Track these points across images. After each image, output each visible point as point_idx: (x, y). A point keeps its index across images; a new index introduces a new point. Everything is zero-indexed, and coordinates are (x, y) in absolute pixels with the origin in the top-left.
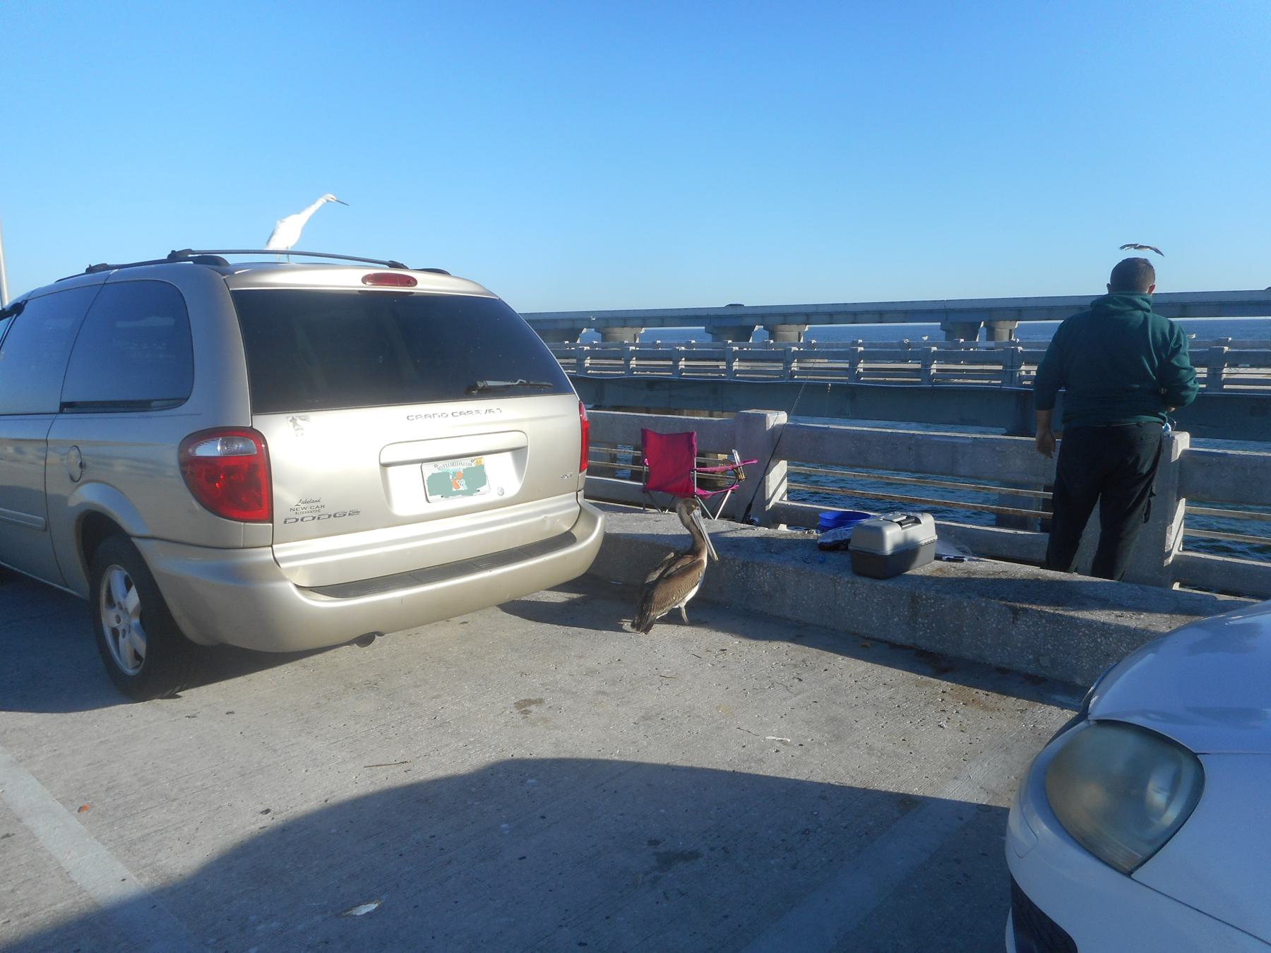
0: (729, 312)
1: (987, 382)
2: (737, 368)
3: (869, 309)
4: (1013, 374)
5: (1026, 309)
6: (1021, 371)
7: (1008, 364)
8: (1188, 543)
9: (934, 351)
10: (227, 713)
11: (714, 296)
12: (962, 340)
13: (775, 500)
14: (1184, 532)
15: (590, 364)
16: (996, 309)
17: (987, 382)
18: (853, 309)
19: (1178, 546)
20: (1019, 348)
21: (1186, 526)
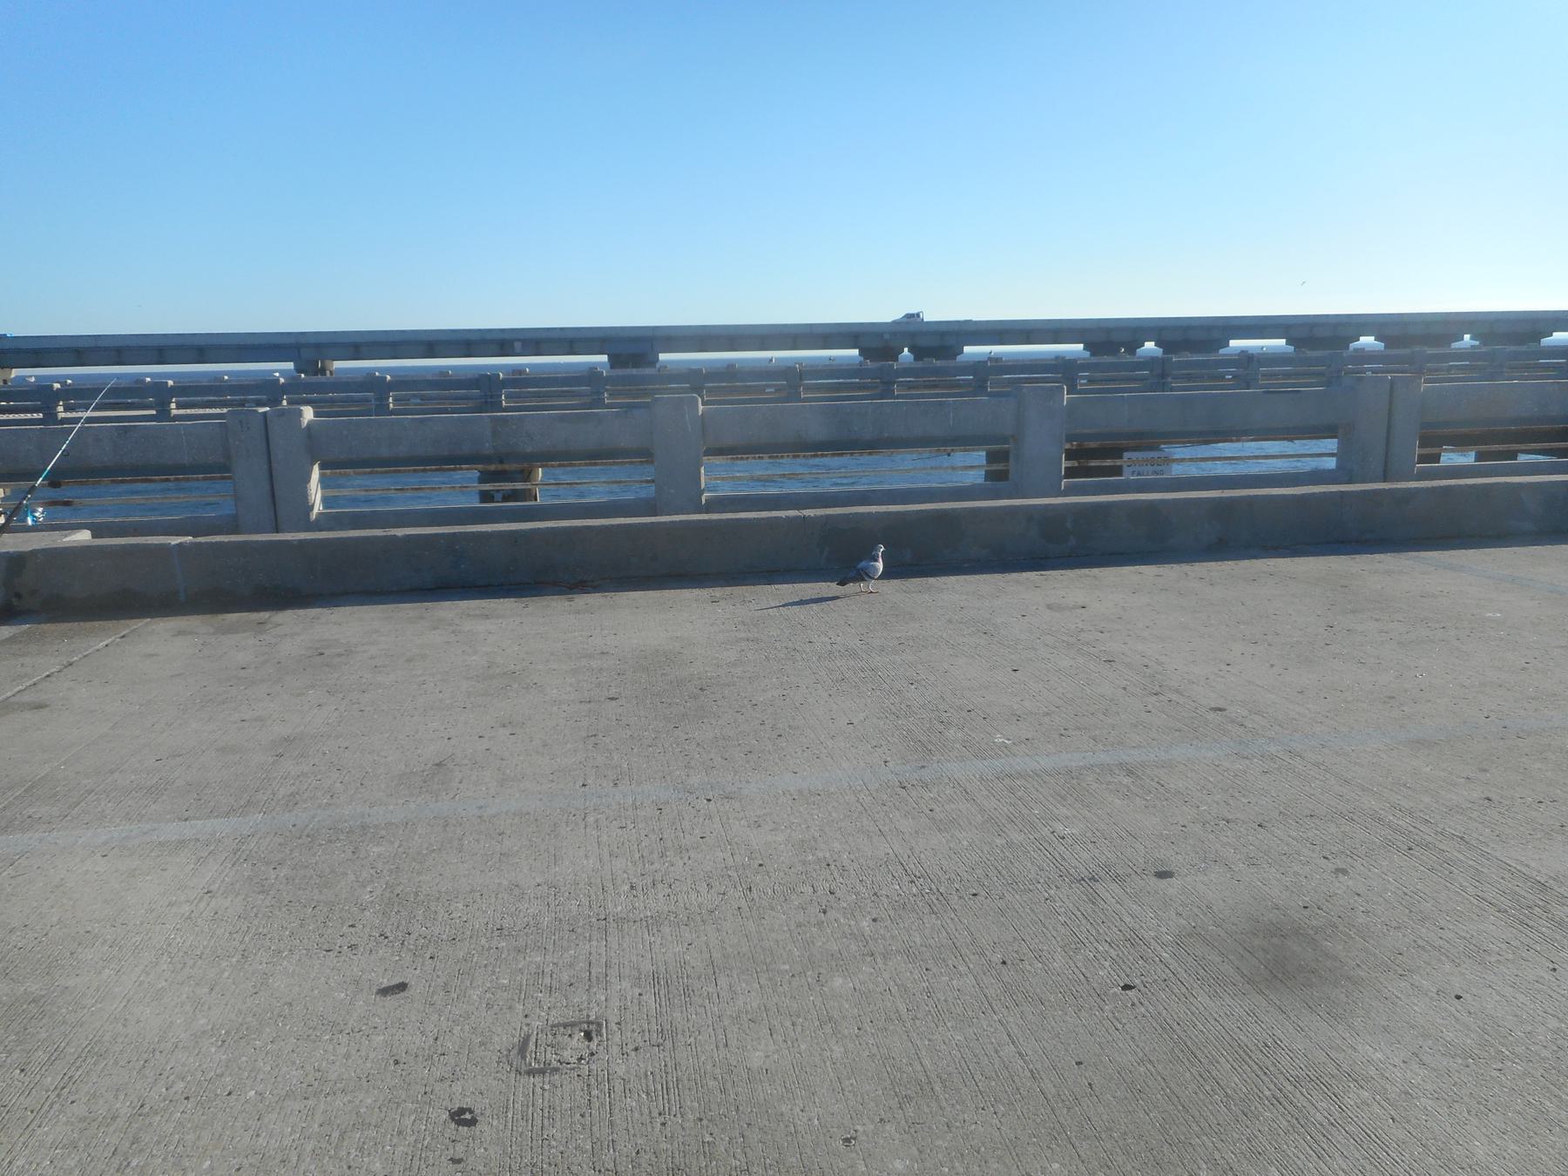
8: (325, 500)
21: (322, 488)
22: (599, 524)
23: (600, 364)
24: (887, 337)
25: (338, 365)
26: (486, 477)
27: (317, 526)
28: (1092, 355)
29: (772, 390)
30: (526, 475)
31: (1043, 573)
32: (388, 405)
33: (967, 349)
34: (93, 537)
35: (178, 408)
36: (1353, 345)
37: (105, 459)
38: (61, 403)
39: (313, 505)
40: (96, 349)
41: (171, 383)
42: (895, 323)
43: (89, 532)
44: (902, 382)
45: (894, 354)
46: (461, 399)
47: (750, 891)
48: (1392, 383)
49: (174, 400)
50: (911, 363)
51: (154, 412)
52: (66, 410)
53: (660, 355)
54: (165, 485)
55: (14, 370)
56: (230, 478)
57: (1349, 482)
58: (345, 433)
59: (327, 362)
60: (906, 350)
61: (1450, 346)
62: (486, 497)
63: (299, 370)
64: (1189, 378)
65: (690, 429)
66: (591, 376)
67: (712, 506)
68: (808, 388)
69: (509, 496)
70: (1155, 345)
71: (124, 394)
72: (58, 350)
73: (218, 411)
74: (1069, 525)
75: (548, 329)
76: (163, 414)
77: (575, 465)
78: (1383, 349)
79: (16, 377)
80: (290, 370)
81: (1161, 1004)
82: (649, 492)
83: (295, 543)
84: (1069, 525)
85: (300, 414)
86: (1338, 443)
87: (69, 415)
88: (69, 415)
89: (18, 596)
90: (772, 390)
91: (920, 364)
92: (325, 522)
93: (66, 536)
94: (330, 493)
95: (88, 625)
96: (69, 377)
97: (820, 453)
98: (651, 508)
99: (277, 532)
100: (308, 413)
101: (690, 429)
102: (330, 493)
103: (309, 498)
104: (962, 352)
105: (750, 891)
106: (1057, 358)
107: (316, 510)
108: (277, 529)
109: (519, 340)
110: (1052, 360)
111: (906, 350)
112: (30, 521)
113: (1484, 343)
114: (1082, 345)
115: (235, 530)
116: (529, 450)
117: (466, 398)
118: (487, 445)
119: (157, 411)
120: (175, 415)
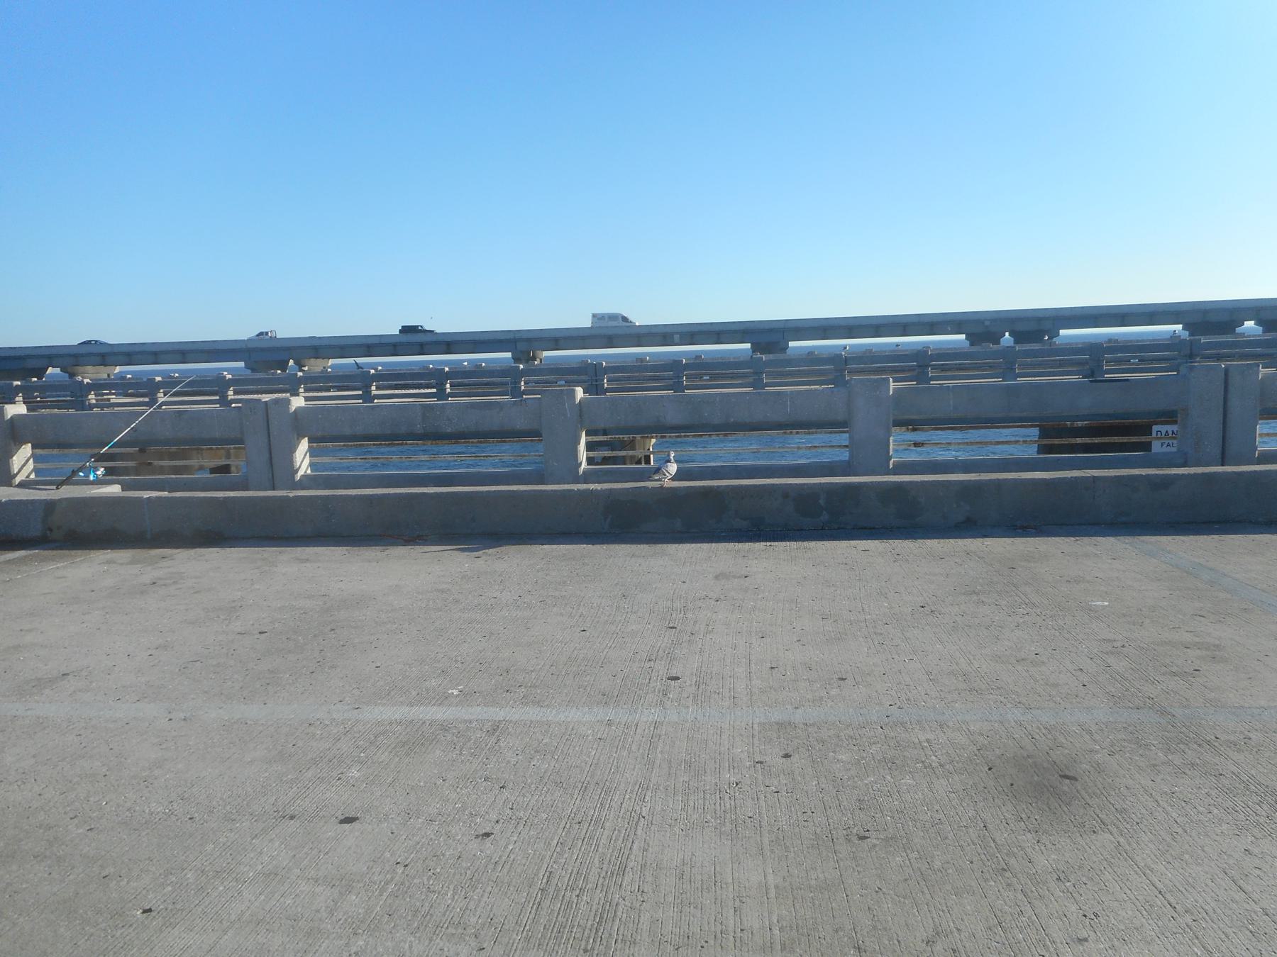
0: (85, 350)
1: (1077, 377)
2: (233, 397)
3: (170, 349)
4: (83, 402)
5: (457, 342)
6: (89, 400)
7: (78, 395)
8: (590, 461)
9: (373, 374)
10: (260, 633)
11: (240, 329)
12: (279, 372)
13: (301, 473)
14: (587, 455)
15: (97, 400)
16: (536, 340)
17: (1077, 377)
18: (154, 349)
19: (305, 469)
20: (156, 378)
21: (587, 451)
22: (737, 484)
23: (746, 350)
24: (987, 323)
25: (546, 354)
26: (1044, 433)
27: (302, 485)
28: (972, 344)
29: (705, 378)
30: (1146, 429)
31: (772, 543)
32: (603, 384)
33: (1063, 332)
34: (122, 491)
35: (234, 394)
36: (1238, 330)
37: (167, 433)
38: (302, 386)
39: (581, 463)
40: (860, 327)
41: (447, 369)
42: (250, 340)
43: (120, 486)
44: (935, 365)
45: (996, 338)
46: (1163, 360)
47: (338, 780)
48: (1226, 371)
49: (374, 384)
50: (1259, 336)
51: (361, 393)
52: (234, 394)
53: (1061, 331)
54: (400, 448)
55: (118, 367)
56: (244, 448)
57: (1185, 465)
58: (320, 416)
59: (539, 352)
60: (1007, 334)
61: (1235, 330)
62: (1044, 449)
63: (516, 359)
64: (943, 368)
65: (569, 415)
66: (1173, 344)
67: (902, 468)
68: (934, 367)
69: (177, 470)
70: (61, 371)
71: (199, 386)
72: (462, 342)
73: (141, 399)
74: (822, 502)
75: (36, 347)
76: (367, 397)
77: (813, 433)
78: (750, 352)
79: (120, 372)
80: (242, 368)
81: (561, 905)
82: (844, 455)
83: (221, 499)
84: (822, 502)
85: (573, 393)
86: (1040, 431)
87: (237, 397)
88: (237, 397)
89: (51, 530)
90: (705, 378)
91: (975, 349)
92: (308, 482)
93: (100, 488)
94: (592, 454)
95: (73, 552)
96: (380, 364)
97: (683, 434)
98: (846, 469)
99: (274, 490)
100: (580, 393)
101: (569, 415)
102: (592, 454)
103: (295, 464)
104: (1058, 335)
105: (338, 780)
106: (1110, 341)
107: (301, 473)
108: (274, 487)
109: (677, 333)
110: (1167, 340)
111: (1007, 334)
112: (91, 478)
113: (1266, 330)
114: (1181, 325)
115: (246, 489)
116: (449, 430)
117: (502, 384)
118: (418, 426)
119: (150, 399)
120: (231, 399)
